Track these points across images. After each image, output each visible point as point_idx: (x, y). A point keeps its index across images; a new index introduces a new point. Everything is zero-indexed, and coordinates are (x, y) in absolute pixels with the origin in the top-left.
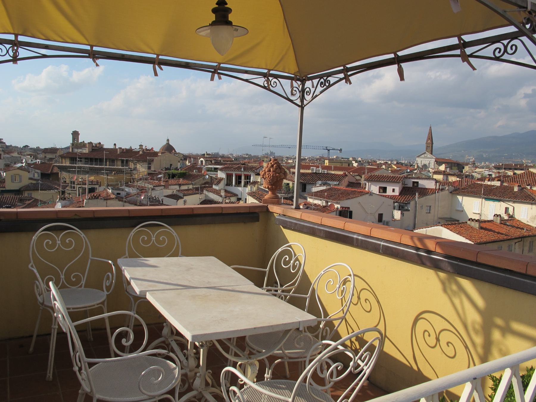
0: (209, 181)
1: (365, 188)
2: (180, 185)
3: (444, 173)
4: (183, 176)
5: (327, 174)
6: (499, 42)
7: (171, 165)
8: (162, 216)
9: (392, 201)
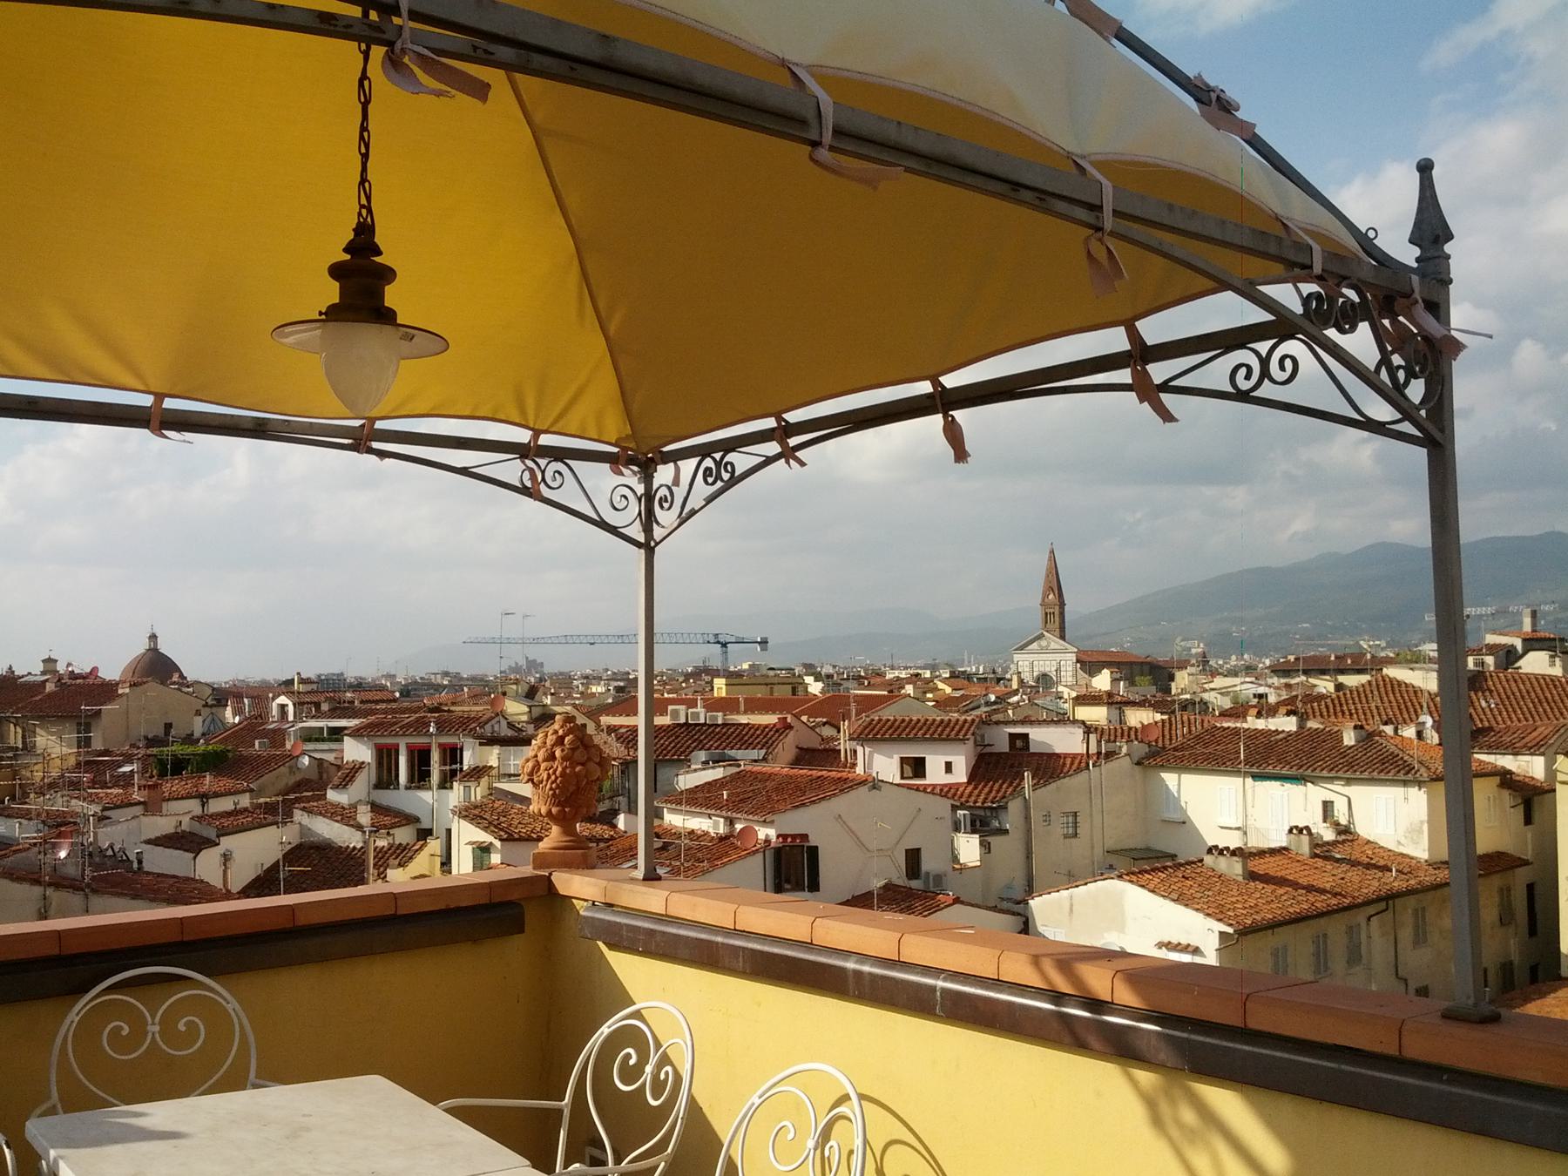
0: (314, 776)
1: (854, 765)
2: (204, 798)
3: (1108, 699)
4: (217, 763)
5: (724, 725)
6: (1242, 346)
7: (168, 726)
8: (183, 943)
9: (948, 803)
